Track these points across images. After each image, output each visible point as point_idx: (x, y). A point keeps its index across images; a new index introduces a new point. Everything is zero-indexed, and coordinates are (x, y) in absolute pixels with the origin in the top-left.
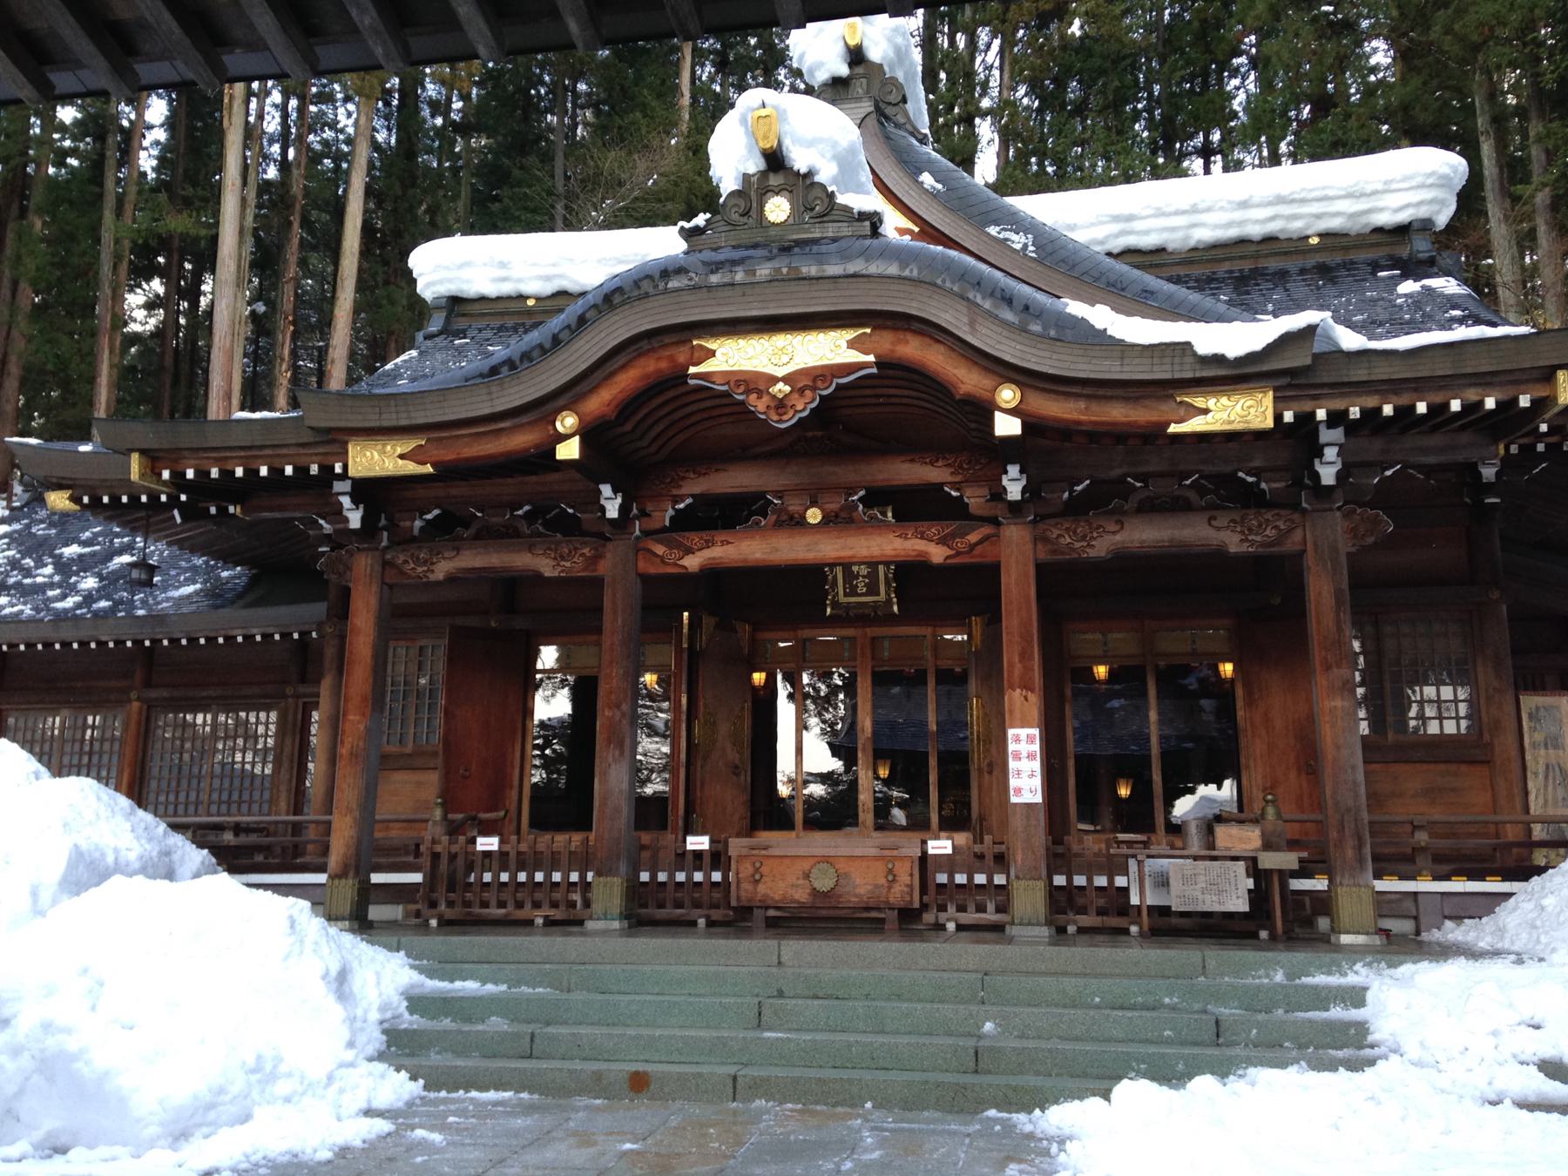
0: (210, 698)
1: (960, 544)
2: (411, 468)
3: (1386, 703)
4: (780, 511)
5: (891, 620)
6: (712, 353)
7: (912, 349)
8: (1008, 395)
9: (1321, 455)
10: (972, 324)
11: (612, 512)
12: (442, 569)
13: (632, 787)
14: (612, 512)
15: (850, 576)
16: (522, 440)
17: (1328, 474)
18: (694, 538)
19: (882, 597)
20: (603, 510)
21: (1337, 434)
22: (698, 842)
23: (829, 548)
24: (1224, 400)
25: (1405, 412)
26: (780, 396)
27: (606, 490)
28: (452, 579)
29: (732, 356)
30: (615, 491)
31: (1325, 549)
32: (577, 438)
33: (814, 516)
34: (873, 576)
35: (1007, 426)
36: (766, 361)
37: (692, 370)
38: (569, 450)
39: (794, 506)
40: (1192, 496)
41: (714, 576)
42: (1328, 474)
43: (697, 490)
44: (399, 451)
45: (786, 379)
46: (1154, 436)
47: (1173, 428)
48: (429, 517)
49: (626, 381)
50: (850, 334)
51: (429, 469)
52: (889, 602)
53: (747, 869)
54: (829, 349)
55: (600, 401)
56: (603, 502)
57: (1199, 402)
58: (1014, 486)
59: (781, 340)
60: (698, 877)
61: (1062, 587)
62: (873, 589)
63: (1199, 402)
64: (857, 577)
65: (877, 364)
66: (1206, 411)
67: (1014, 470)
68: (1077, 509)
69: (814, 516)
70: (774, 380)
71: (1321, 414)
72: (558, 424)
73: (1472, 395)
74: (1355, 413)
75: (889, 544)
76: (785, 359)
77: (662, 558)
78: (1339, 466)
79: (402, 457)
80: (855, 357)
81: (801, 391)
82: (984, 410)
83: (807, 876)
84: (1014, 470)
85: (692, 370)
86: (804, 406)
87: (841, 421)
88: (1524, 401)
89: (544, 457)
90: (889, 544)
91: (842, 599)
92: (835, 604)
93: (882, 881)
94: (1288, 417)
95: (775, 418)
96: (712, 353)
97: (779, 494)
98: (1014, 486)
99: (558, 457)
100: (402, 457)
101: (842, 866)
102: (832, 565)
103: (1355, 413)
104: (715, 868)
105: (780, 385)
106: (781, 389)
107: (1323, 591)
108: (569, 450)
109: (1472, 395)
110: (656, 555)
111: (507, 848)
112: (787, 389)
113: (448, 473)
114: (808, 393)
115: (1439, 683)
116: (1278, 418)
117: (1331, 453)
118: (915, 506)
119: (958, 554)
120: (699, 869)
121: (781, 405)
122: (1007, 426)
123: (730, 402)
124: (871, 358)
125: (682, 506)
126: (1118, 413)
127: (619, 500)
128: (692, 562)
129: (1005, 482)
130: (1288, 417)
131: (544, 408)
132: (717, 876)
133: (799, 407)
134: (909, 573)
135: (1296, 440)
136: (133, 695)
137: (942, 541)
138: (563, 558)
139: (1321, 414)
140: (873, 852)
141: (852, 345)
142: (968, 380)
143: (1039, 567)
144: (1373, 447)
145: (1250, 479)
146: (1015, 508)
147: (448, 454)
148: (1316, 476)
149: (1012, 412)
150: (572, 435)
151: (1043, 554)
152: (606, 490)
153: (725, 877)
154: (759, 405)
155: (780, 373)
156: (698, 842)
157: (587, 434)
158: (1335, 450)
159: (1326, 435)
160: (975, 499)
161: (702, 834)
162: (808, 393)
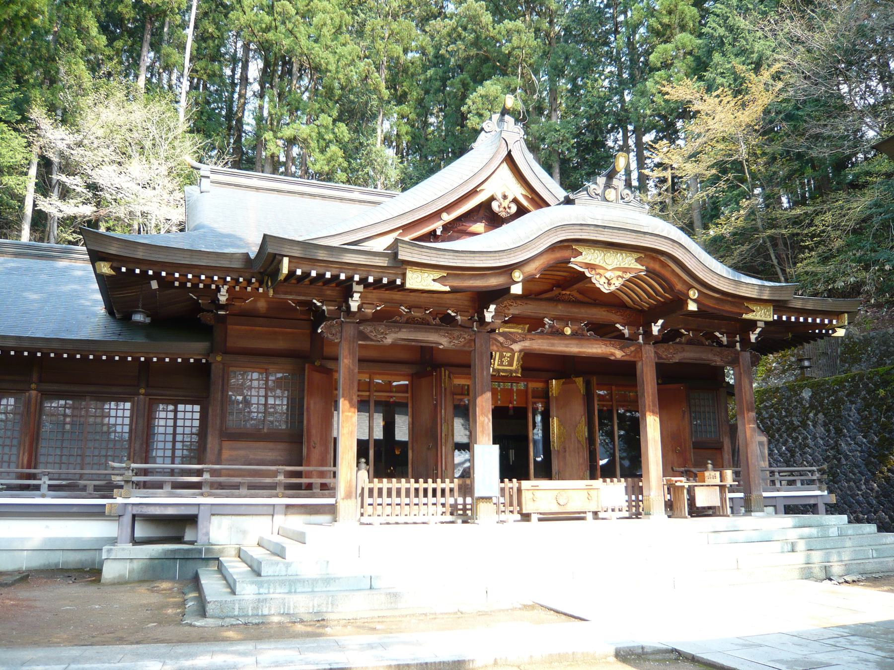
0: (88, 392)
1: (628, 351)
6: (581, 254)
9: (352, 297)
12: (389, 340)
13: (473, 456)
16: (494, 282)
19: (514, 367)
21: (360, 288)
28: (393, 346)
33: (568, 331)
37: (572, 260)
40: (430, 319)
42: (354, 305)
43: (516, 312)
44: (432, 277)
47: (744, 316)
50: (636, 256)
57: (751, 306)
62: (511, 364)
77: (501, 344)
79: (434, 280)
100: (434, 280)
108: (516, 289)
110: (499, 342)
117: (356, 296)
119: (627, 355)
131: (508, 269)
136: (33, 386)
137: (621, 349)
141: (637, 260)
143: (657, 364)
144: (374, 295)
145: (453, 314)
147: (458, 283)
148: (349, 307)
149: (694, 300)
151: (657, 360)
158: (359, 295)
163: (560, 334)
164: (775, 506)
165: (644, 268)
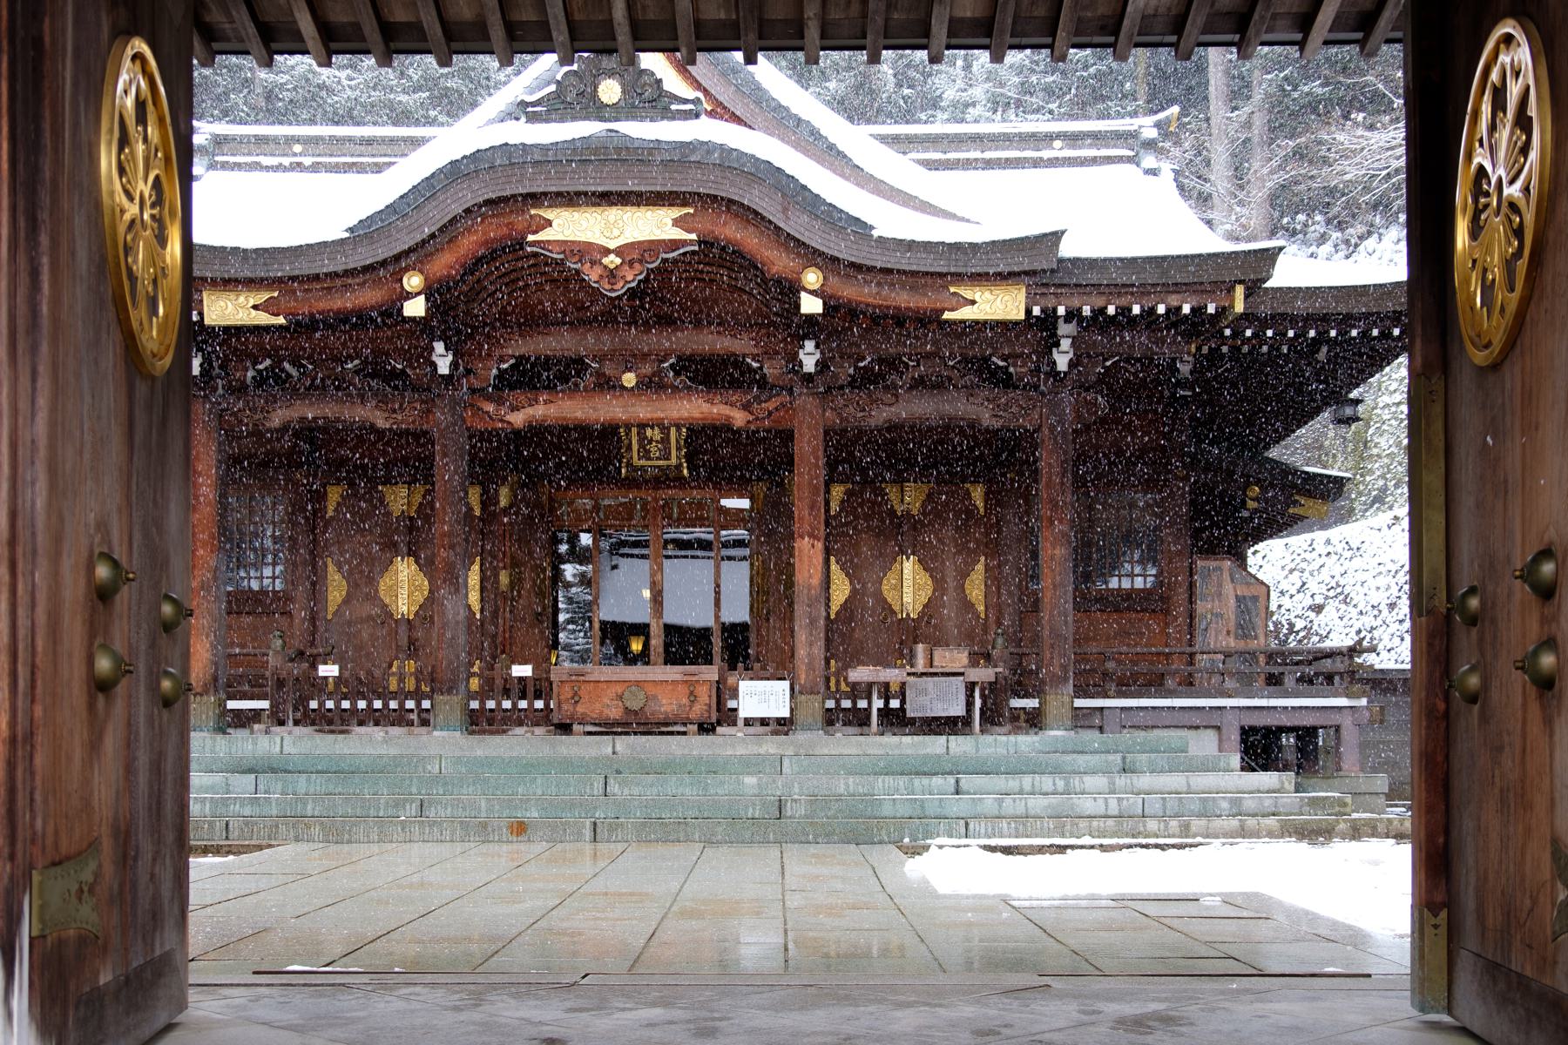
2: (264, 319)
3: (1090, 560)
4: (599, 374)
5: (680, 482)
6: (549, 223)
7: (731, 231)
8: (812, 278)
9: (1057, 345)
10: (785, 210)
11: (444, 367)
14: (444, 367)
15: (642, 438)
16: (367, 296)
17: (1062, 362)
18: (520, 396)
19: (674, 461)
20: (434, 366)
22: (522, 671)
23: (643, 410)
24: (987, 295)
25: (1124, 311)
26: (612, 266)
27: (439, 347)
29: (567, 226)
30: (447, 349)
31: (1053, 422)
32: (422, 298)
33: (629, 379)
34: (665, 440)
35: (811, 305)
36: (598, 234)
37: (531, 238)
38: (415, 308)
39: (609, 370)
41: (536, 433)
43: (522, 351)
44: (252, 302)
45: (619, 252)
46: (930, 320)
47: (947, 315)
48: (261, 367)
49: (469, 244)
50: (676, 212)
51: (281, 320)
52: (678, 467)
53: (567, 692)
54: (655, 225)
55: (445, 263)
56: (434, 358)
57: (967, 293)
58: (809, 357)
59: (614, 213)
60: (523, 704)
61: (844, 451)
63: (967, 293)
64: (650, 442)
65: (700, 242)
66: (973, 302)
67: (809, 345)
68: (864, 380)
69: (629, 379)
70: (607, 251)
71: (1061, 311)
72: (405, 280)
73: (1174, 300)
74: (1086, 311)
75: (695, 407)
76: (616, 232)
78: (1071, 355)
79: (255, 307)
80: (678, 234)
81: (631, 264)
82: (791, 290)
83: (620, 697)
84: (809, 345)
85: (531, 238)
86: (632, 277)
87: (661, 292)
88: (1211, 309)
89: (391, 311)
90: (695, 407)
91: (636, 462)
92: (629, 464)
93: (685, 701)
94: (1036, 311)
95: (608, 287)
96: (549, 223)
97: (601, 358)
98: (809, 357)
99: (423, 314)
100: (255, 307)
101: (651, 690)
102: (628, 427)
103: (1086, 311)
104: (538, 696)
105: (612, 257)
106: (612, 261)
107: (1049, 461)
108: (415, 308)
109: (1174, 300)
111: (347, 674)
112: (618, 261)
113: (301, 328)
114: (637, 265)
115: (1120, 589)
116: (1028, 312)
117: (1065, 344)
118: (709, 373)
120: (523, 697)
121: (612, 274)
122: (811, 305)
123: (562, 273)
124: (694, 236)
125: (505, 366)
126: (903, 299)
127: (450, 357)
128: (518, 419)
129: (801, 356)
130: (1036, 311)
131: (396, 264)
132: (539, 704)
133: (630, 278)
134: (700, 437)
135: (1042, 328)
137: (746, 407)
138: (394, 411)
139: (1061, 311)
140: (678, 677)
141: (677, 222)
142: (779, 262)
145: (1001, 364)
146: (809, 378)
150: (418, 294)
152: (439, 347)
153: (547, 705)
154: (592, 275)
155: (612, 245)
156: (522, 671)
157: (428, 292)
159: (1064, 329)
160: (771, 370)
161: (526, 663)
162: (637, 265)
163: (608, 384)
164: (1218, 728)
165: (694, 236)
